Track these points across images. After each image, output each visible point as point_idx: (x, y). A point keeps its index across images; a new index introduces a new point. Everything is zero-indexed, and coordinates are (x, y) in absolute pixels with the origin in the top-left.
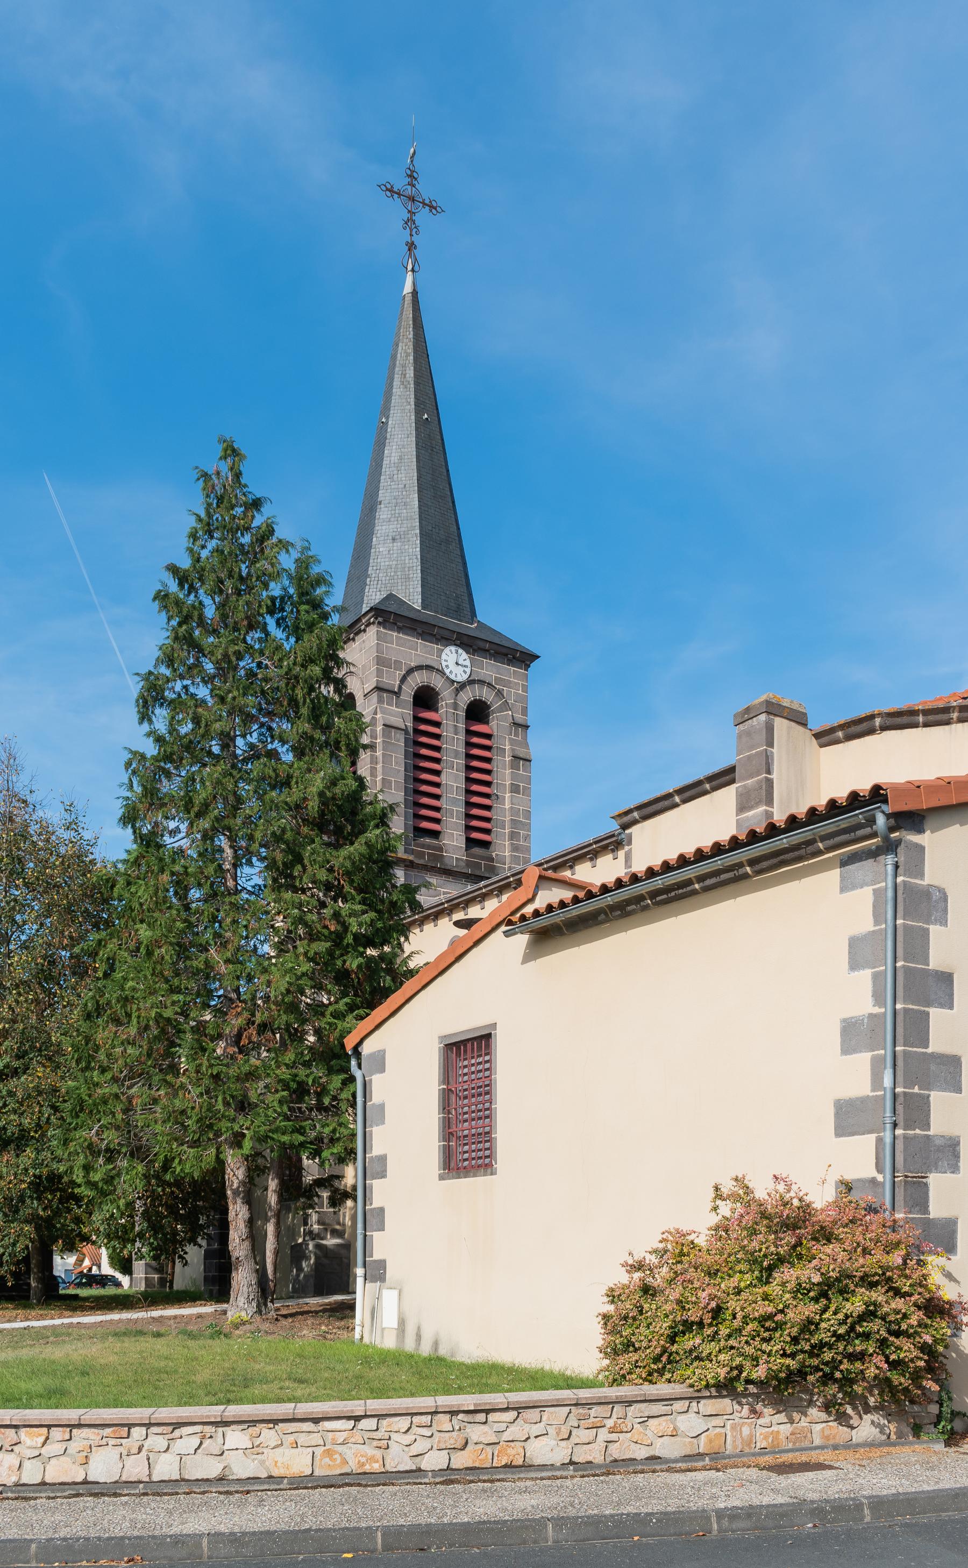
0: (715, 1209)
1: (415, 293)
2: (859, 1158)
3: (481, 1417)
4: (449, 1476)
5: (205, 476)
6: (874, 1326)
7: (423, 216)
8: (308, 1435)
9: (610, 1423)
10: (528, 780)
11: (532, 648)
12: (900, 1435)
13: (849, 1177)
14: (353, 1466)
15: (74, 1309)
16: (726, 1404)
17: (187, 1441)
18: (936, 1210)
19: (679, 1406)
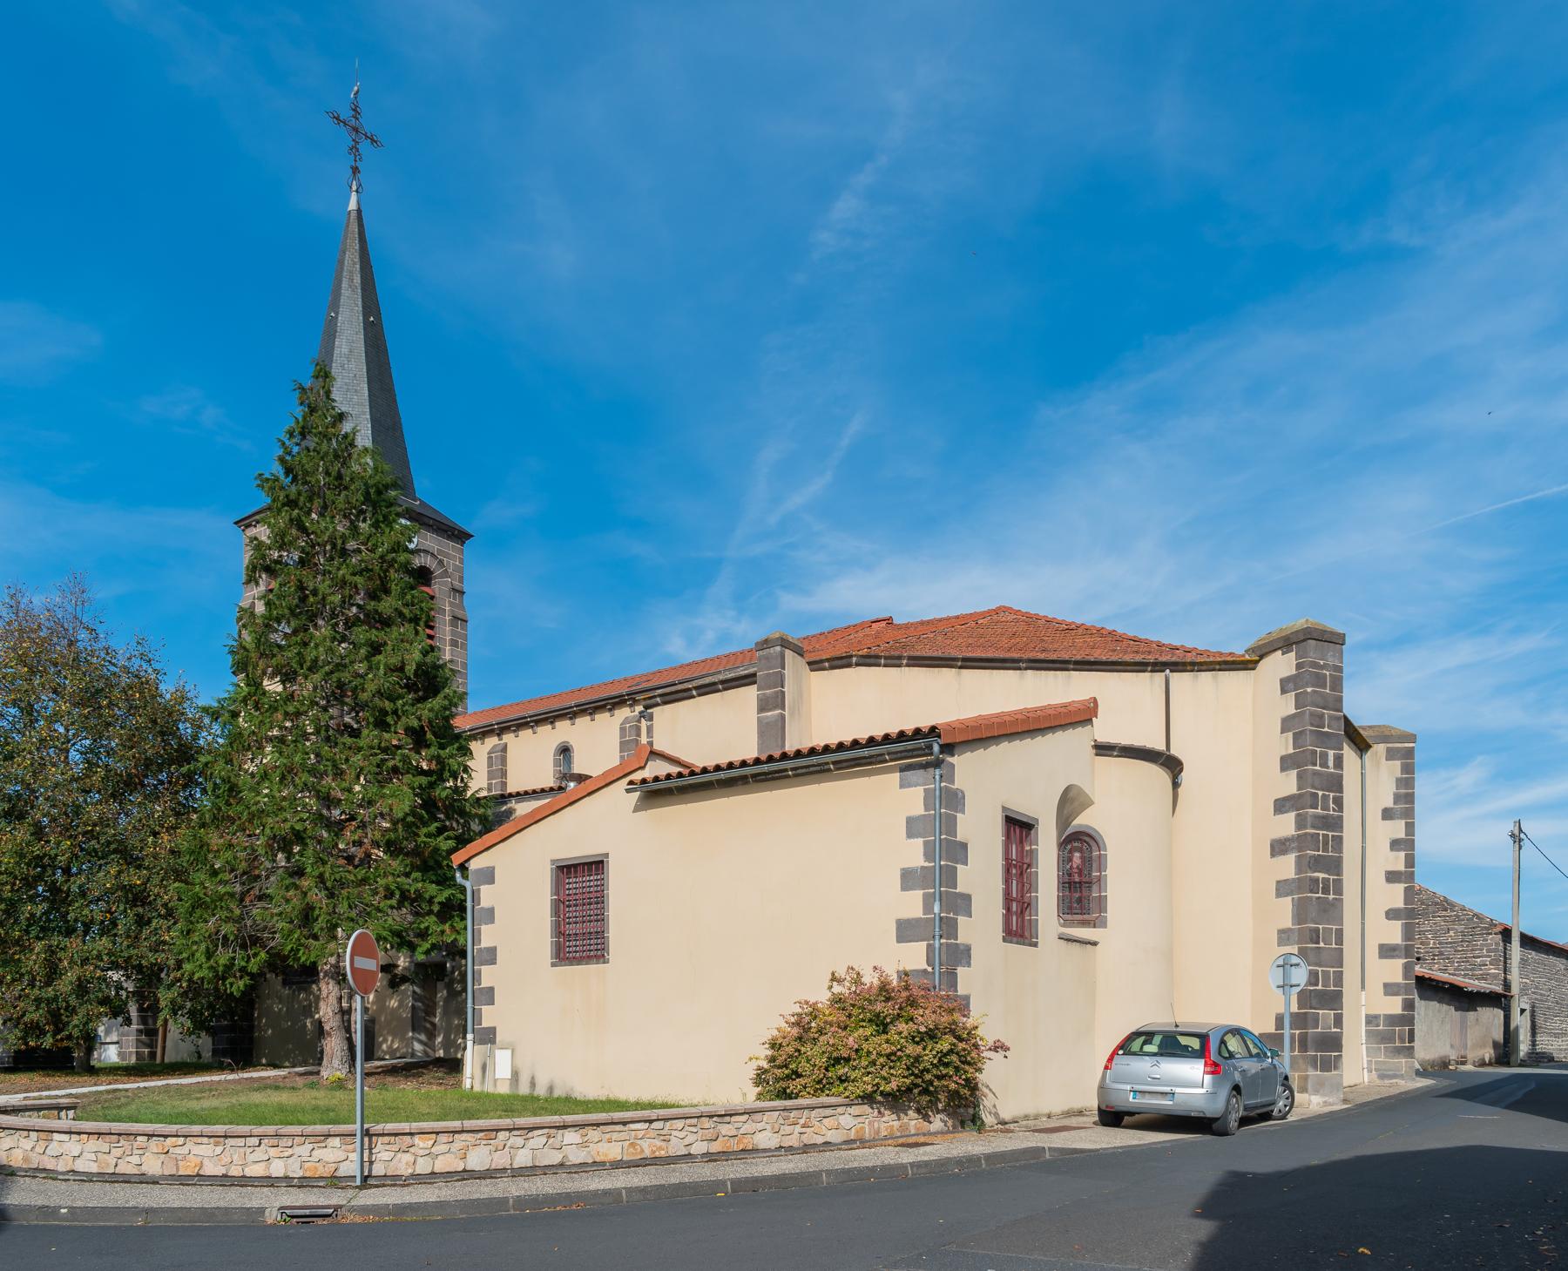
0: (831, 987)
1: (359, 211)
2: (914, 956)
3: (727, 1119)
4: (710, 1157)
5: (303, 389)
6: (954, 1058)
7: (364, 146)
8: (618, 1133)
9: (802, 1121)
10: (465, 637)
11: (470, 531)
12: (954, 1127)
13: (908, 968)
14: (647, 1153)
15: (93, 1079)
16: (866, 1108)
17: (538, 1139)
18: (962, 990)
19: (840, 1110)
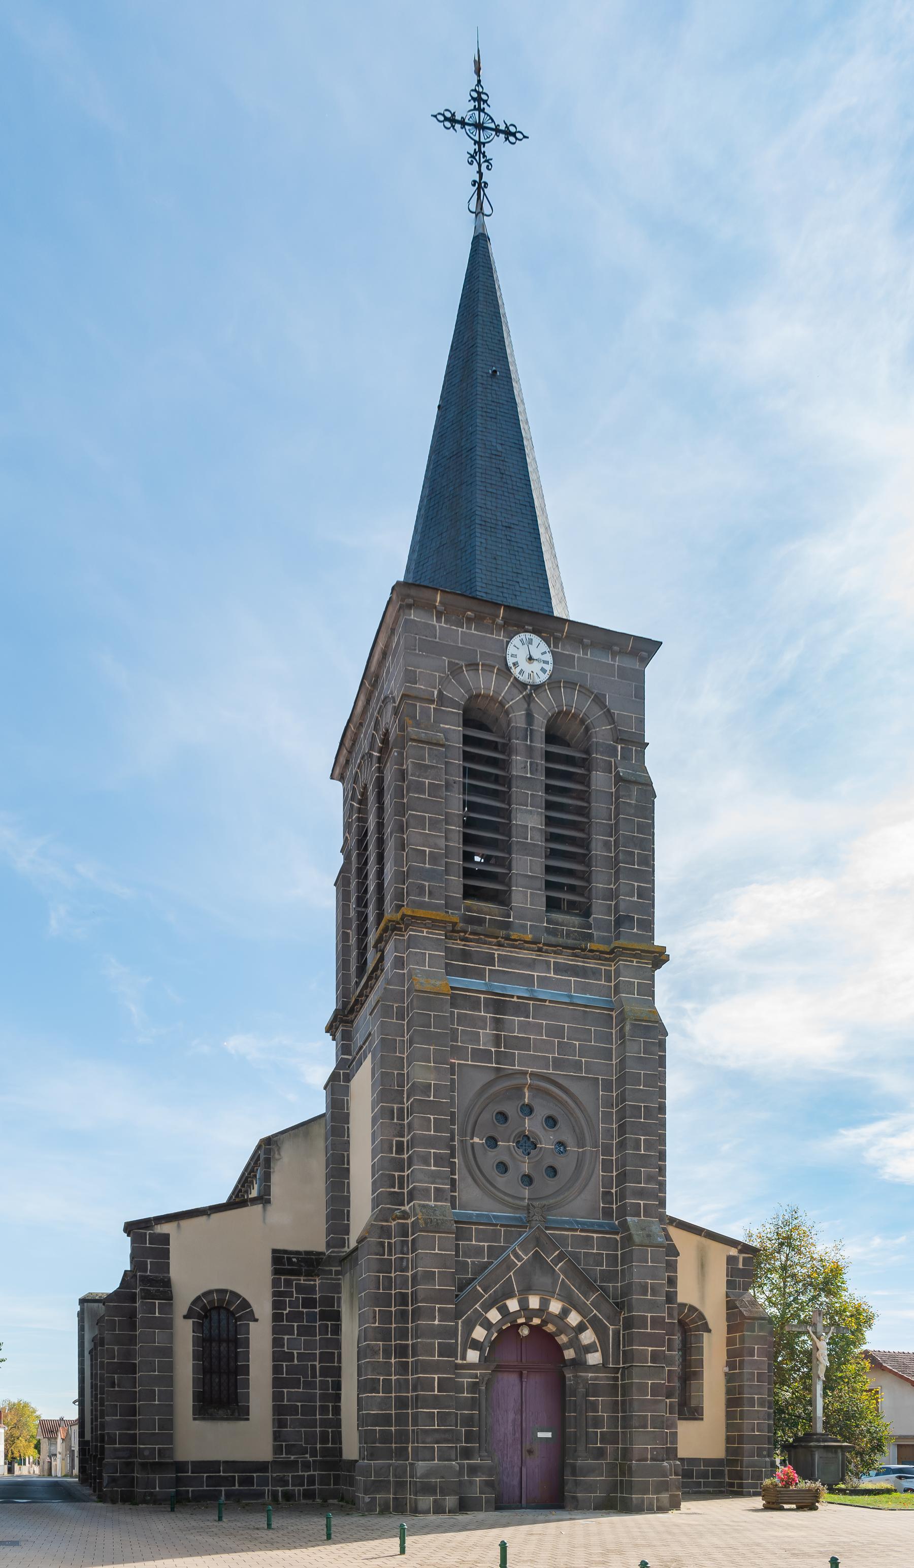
7: (496, 147)
